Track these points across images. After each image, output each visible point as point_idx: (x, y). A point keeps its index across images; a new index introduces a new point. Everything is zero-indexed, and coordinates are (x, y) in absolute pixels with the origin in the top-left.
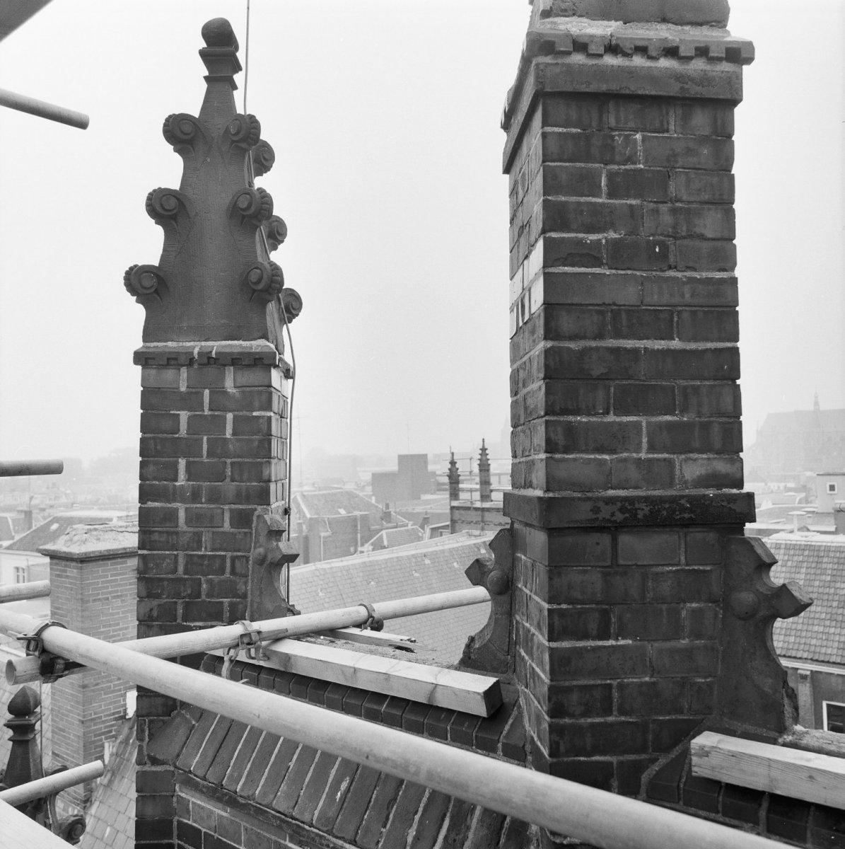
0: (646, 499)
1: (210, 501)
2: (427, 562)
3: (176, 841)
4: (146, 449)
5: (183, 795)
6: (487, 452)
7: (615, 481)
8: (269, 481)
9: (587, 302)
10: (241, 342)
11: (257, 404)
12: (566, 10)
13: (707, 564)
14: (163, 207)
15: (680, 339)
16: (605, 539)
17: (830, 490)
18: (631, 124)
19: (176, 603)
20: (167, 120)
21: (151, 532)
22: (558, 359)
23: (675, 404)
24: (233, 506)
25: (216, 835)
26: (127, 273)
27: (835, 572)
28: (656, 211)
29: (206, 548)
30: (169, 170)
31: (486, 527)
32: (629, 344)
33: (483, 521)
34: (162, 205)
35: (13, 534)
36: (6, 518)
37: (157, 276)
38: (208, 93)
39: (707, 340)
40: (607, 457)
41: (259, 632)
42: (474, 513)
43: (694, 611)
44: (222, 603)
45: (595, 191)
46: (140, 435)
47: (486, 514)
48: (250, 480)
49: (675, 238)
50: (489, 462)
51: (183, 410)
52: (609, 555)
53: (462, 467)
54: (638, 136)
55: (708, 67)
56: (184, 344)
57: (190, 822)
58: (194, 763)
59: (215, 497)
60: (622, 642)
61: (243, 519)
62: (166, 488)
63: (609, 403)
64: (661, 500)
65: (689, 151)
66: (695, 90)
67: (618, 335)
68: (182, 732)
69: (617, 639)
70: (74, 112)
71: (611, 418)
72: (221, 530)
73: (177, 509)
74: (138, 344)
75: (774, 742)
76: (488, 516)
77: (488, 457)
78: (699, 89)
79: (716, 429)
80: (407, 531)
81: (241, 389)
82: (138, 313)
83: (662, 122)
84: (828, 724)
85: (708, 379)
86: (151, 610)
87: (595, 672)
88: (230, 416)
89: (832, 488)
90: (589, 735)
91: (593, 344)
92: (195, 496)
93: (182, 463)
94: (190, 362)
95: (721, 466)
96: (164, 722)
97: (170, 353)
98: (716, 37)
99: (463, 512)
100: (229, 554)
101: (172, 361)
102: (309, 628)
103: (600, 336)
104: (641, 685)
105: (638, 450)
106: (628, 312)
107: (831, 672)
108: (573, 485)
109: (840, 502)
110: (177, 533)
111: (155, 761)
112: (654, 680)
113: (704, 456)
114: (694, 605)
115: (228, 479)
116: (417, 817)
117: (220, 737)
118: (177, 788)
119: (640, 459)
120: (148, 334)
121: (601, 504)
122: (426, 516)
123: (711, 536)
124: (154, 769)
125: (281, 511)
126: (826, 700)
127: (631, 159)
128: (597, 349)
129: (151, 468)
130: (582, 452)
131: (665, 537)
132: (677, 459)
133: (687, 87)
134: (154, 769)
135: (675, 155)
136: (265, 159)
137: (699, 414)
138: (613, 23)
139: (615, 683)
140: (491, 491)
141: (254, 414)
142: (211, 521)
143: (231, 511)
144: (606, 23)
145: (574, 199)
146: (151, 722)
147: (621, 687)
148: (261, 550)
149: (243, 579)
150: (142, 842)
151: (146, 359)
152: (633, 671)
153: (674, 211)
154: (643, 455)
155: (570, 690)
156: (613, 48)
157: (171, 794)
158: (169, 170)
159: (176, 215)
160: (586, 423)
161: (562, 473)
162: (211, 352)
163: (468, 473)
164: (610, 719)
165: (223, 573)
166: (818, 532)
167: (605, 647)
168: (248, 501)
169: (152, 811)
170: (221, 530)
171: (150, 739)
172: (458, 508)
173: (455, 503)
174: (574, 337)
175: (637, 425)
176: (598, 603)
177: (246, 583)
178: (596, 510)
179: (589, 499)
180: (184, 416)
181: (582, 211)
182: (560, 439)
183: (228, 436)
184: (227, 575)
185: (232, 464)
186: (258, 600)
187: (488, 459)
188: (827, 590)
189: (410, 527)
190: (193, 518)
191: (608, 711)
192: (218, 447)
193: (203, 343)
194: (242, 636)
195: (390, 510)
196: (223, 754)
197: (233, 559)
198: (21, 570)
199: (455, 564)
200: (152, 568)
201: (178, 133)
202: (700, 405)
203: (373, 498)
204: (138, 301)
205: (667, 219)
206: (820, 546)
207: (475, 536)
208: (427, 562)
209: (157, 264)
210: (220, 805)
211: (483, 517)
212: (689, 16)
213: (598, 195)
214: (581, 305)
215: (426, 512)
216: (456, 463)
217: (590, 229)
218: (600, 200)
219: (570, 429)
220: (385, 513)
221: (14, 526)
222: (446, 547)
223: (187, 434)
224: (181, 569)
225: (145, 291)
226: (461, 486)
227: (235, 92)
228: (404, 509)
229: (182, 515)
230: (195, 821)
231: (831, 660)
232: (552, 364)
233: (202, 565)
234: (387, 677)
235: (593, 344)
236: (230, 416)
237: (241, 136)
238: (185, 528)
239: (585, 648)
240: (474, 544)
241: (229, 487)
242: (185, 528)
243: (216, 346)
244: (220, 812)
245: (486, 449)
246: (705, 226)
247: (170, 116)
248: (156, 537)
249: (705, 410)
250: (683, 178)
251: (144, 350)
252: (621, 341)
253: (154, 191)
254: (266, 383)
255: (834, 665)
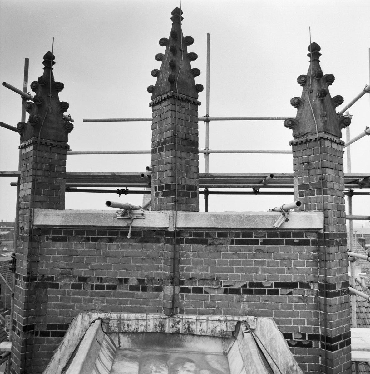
31: (186, 300)
33: (175, 280)
42: (134, 249)
47: (190, 251)
70: (143, 151)
79: (178, 166)
99: (81, 248)
191: (298, 317)
211: (176, 261)
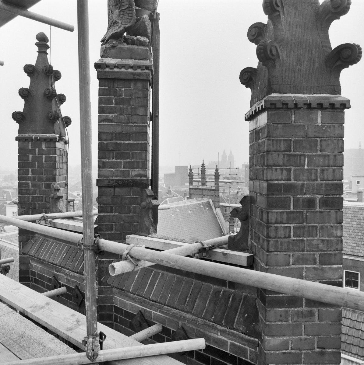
0: (122, 180)
1: (39, 181)
2: (178, 210)
3: (30, 276)
4: (20, 165)
5: (32, 263)
6: (205, 165)
7: (115, 175)
8: (56, 175)
9: (108, 131)
10: (47, 134)
11: (52, 153)
12: (106, 56)
13: (137, 196)
14: (24, 93)
15: (132, 141)
16: (112, 189)
17: (359, 182)
18: (121, 86)
19: (29, 210)
20: (25, 66)
21: (22, 190)
22: (101, 145)
23: (130, 156)
24: (45, 182)
25: (39, 273)
26: (13, 114)
27: (352, 218)
28: (127, 108)
29: (38, 194)
30: (26, 82)
32: (119, 142)
33: (202, 194)
34: (23, 94)
35: (12, 198)
36: (9, 191)
37: (22, 115)
38: (38, 56)
39: (138, 141)
40: (113, 169)
41: (47, 216)
43: (134, 207)
44: (42, 210)
45: (111, 103)
46: (18, 161)
47: (204, 191)
48: (50, 175)
49: (131, 115)
50: (205, 170)
51: (30, 154)
52: (113, 193)
53: (195, 172)
54: (123, 89)
55: (141, 71)
56: (30, 135)
57: (33, 270)
58: (32, 253)
59: (40, 180)
60: (116, 214)
61: (48, 186)
62: (26, 177)
63: (113, 156)
64: (125, 180)
65: (136, 93)
66: (137, 77)
67: (116, 140)
68: (31, 245)
69: (114, 213)
71: (114, 160)
72: (42, 189)
73: (29, 183)
74: (17, 135)
75: (146, 236)
76: (205, 192)
77: (205, 167)
78: (138, 77)
80: (178, 198)
81: (47, 148)
82: (17, 126)
83: (129, 86)
84: (345, 279)
85: (139, 151)
86: (22, 212)
87: (109, 221)
88: (44, 156)
89: (358, 182)
90: (107, 235)
91: (110, 142)
92: (34, 180)
93: (30, 170)
94: (32, 140)
95: (142, 172)
96: (26, 243)
97: (26, 137)
98: (145, 63)
99: (194, 190)
100: (44, 196)
101: (26, 140)
102: (64, 216)
103: (112, 140)
104: (120, 224)
105: (121, 168)
106: (119, 134)
107: (348, 258)
108: (104, 176)
109: (361, 188)
110: (29, 190)
111: (24, 254)
112: (124, 223)
113: (138, 169)
114: (134, 205)
115: (44, 174)
116: (78, 260)
117: (39, 245)
118: (30, 261)
119: (121, 170)
120: (20, 132)
121: (110, 181)
122: (185, 192)
123: (139, 189)
124: (24, 256)
125: (64, 184)
126: (345, 269)
127: (121, 95)
128: (111, 143)
129: (22, 171)
130: (107, 168)
131: (127, 189)
132: (130, 170)
133: (135, 76)
134: (24, 256)
135: (132, 94)
136: (58, 76)
137: (136, 159)
138: (118, 59)
139: (114, 223)
140: (206, 182)
141: (51, 156)
142: (39, 187)
143: (45, 184)
144: (116, 59)
145: (106, 105)
146: (23, 243)
147: (116, 225)
148: (52, 195)
149: (48, 203)
150: (21, 276)
151: (19, 139)
152: (118, 221)
153: (132, 108)
154: (122, 169)
155: (103, 225)
156: (116, 66)
157: (29, 263)
158: (26, 82)
159: (28, 96)
160: (108, 161)
161: (102, 173)
162: (38, 137)
163: (197, 174)
164: (113, 232)
165: (43, 201)
166: (347, 201)
167: (111, 215)
168: (49, 181)
169: (23, 268)
170: (42, 189)
171: (22, 248)
172: (192, 189)
173: (191, 187)
174: (104, 140)
175: (120, 162)
176: (110, 204)
177: (49, 204)
178: (109, 182)
179: (107, 180)
180: (31, 156)
181: (108, 108)
182: (101, 165)
183: (43, 162)
184: (44, 202)
185: (45, 170)
186: (52, 209)
187: (205, 169)
188: (348, 225)
189: (179, 197)
190: (34, 186)
191: (112, 230)
192: (41, 165)
193: (36, 135)
194: (42, 217)
195: (171, 190)
196: (39, 250)
197: (45, 197)
198: (15, 213)
199: (190, 212)
200: (22, 200)
201: (28, 71)
202: (136, 157)
203: (165, 184)
204: (17, 122)
205: (130, 110)
206: (346, 207)
207: (199, 200)
208: (178, 210)
209: (22, 111)
210: (40, 264)
211: (202, 192)
212: (138, 57)
213: (112, 104)
214: (107, 132)
215: (185, 191)
216: (192, 170)
217: (110, 113)
218: (113, 106)
219: (104, 163)
220: (168, 191)
221: (12, 195)
222: (186, 204)
223: (32, 161)
224: (30, 200)
225: (18, 119)
226: (194, 180)
227: (48, 55)
228: (177, 190)
229: (30, 185)
230: (35, 270)
231: (348, 254)
232: (99, 147)
233: (36, 199)
234: (75, 226)
235: (110, 142)
236: (44, 156)
237: (47, 72)
238: (31, 188)
239: (107, 215)
240: (198, 204)
241: (44, 177)
242: (31, 188)
243: (39, 136)
244: (40, 266)
245: (204, 164)
246: (139, 112)
247: (25, 65)
248: (23, 191)
249: (138, 158)
250: (134, 100)
251: (19, 137)
252: (117, 141)
253: (21, 89)
254: (54, 147)
255: (349, 255)
